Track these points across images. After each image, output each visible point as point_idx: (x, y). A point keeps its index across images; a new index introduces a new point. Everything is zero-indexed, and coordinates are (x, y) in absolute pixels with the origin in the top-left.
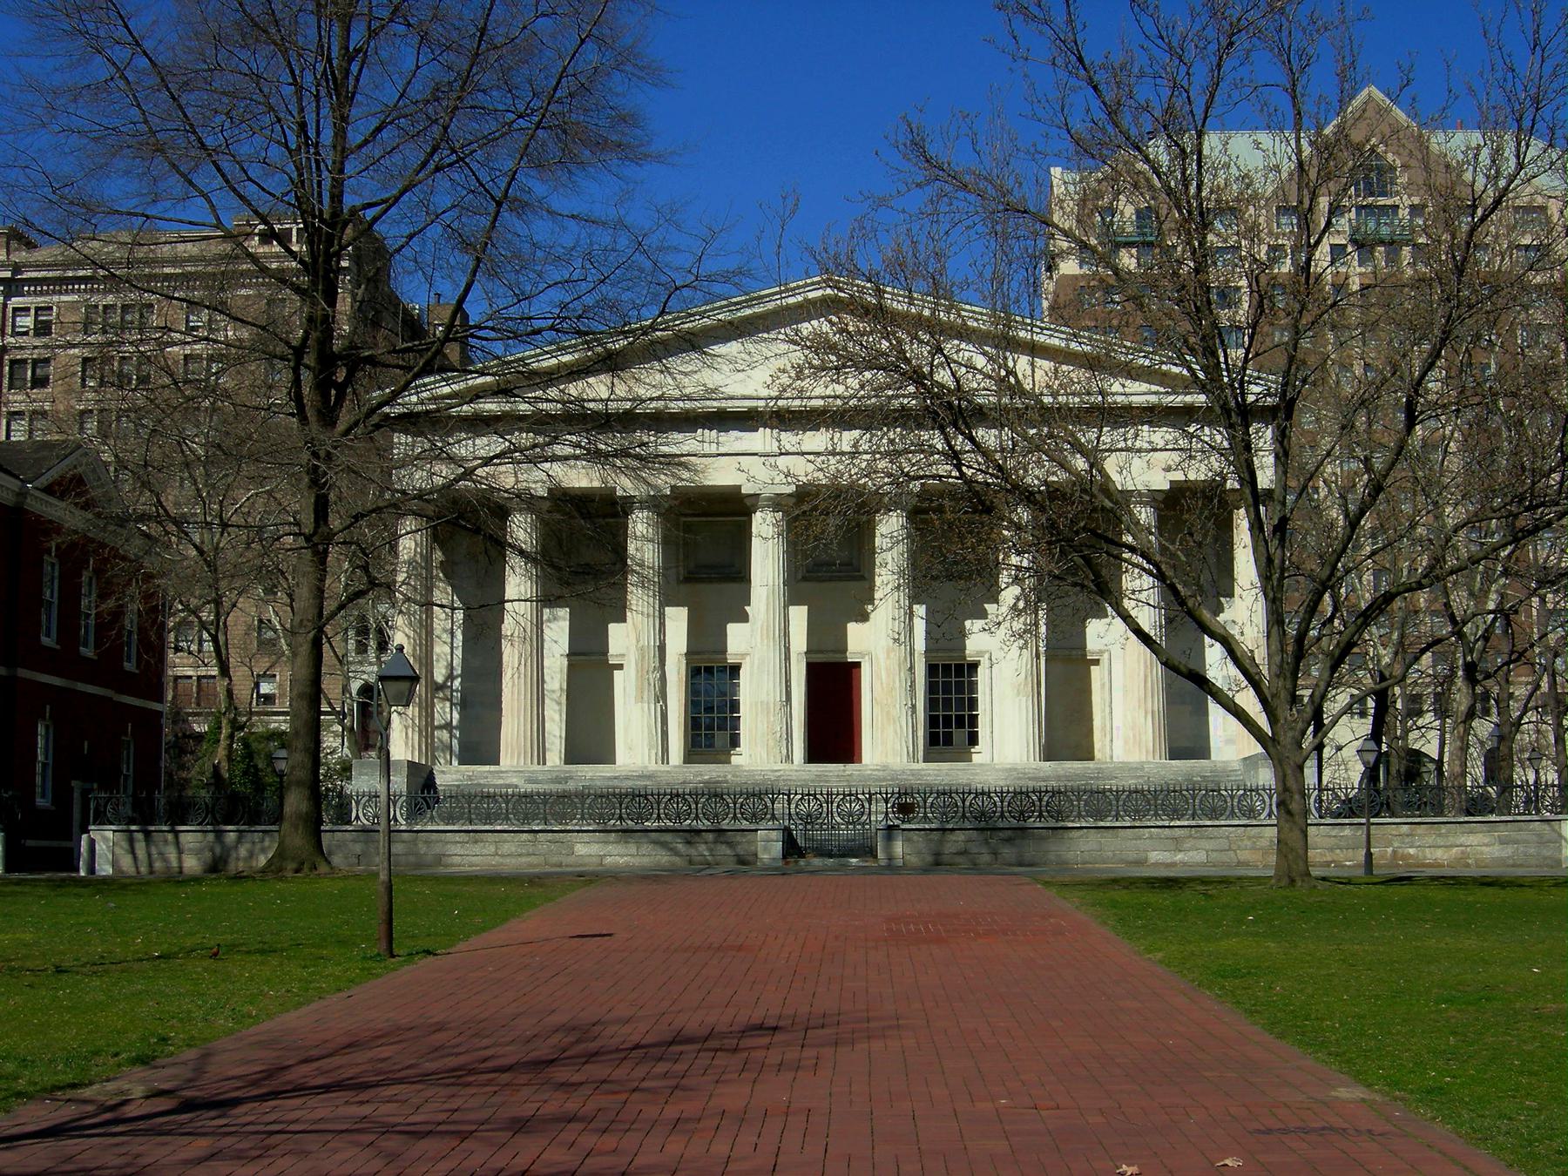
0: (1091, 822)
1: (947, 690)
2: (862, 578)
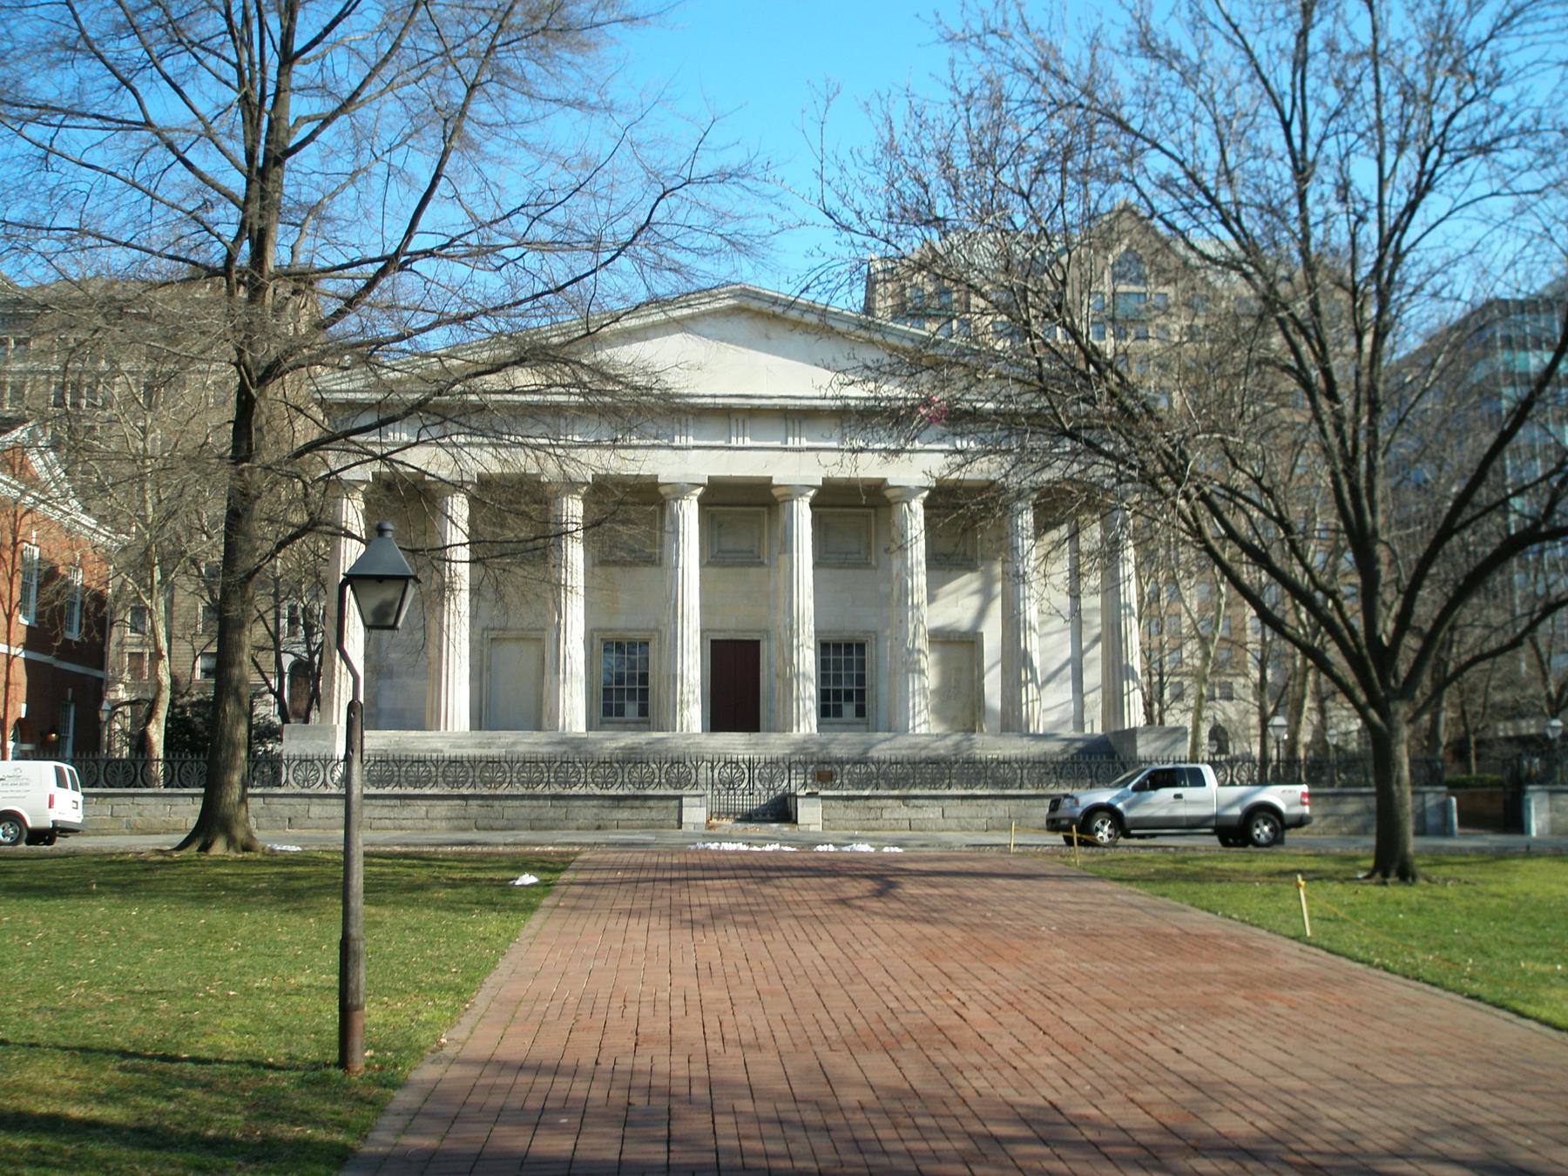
0: (446, 791)
1: (837, 667)
2: (761, 564)
